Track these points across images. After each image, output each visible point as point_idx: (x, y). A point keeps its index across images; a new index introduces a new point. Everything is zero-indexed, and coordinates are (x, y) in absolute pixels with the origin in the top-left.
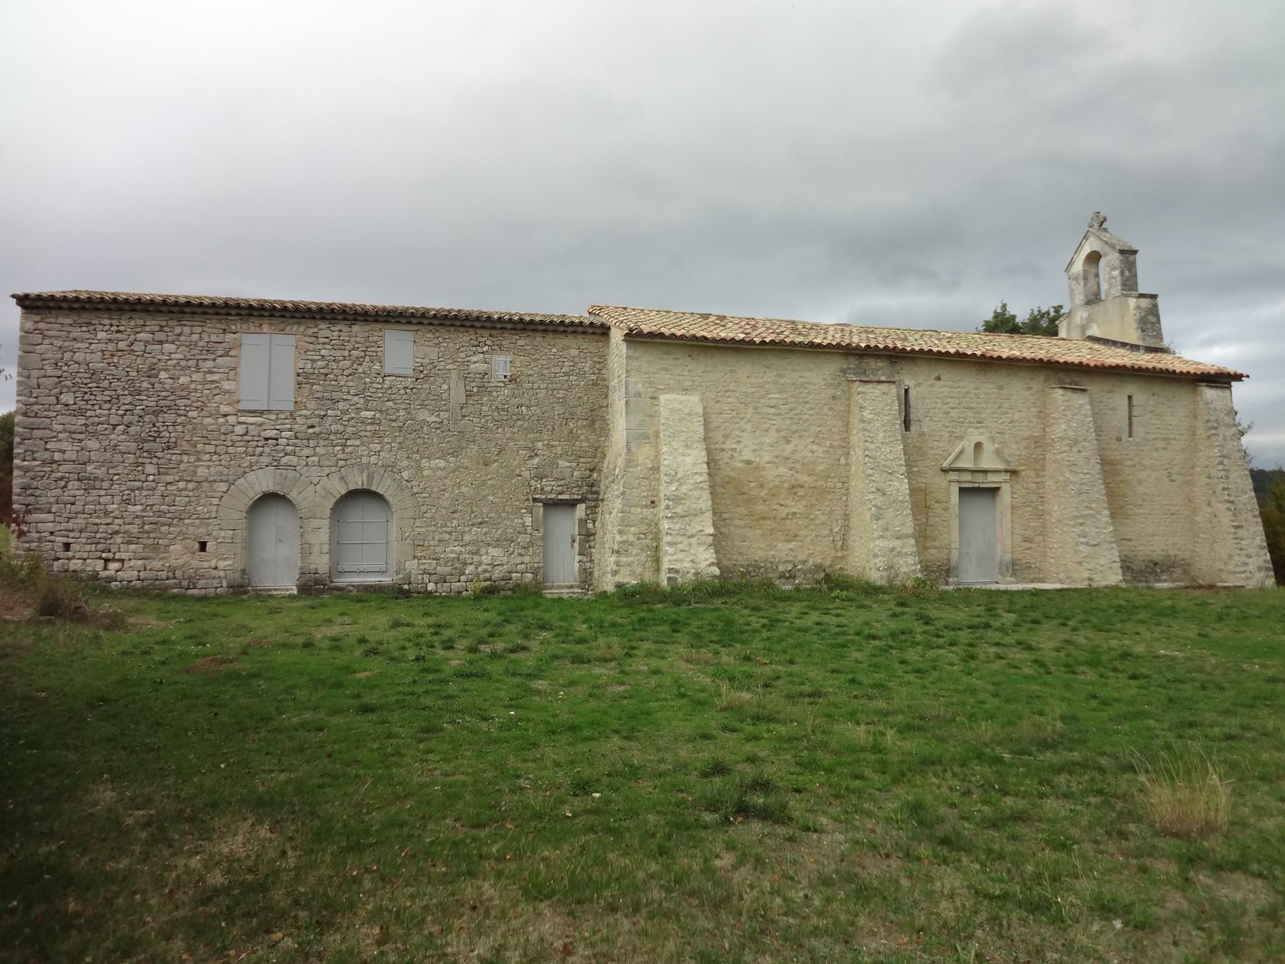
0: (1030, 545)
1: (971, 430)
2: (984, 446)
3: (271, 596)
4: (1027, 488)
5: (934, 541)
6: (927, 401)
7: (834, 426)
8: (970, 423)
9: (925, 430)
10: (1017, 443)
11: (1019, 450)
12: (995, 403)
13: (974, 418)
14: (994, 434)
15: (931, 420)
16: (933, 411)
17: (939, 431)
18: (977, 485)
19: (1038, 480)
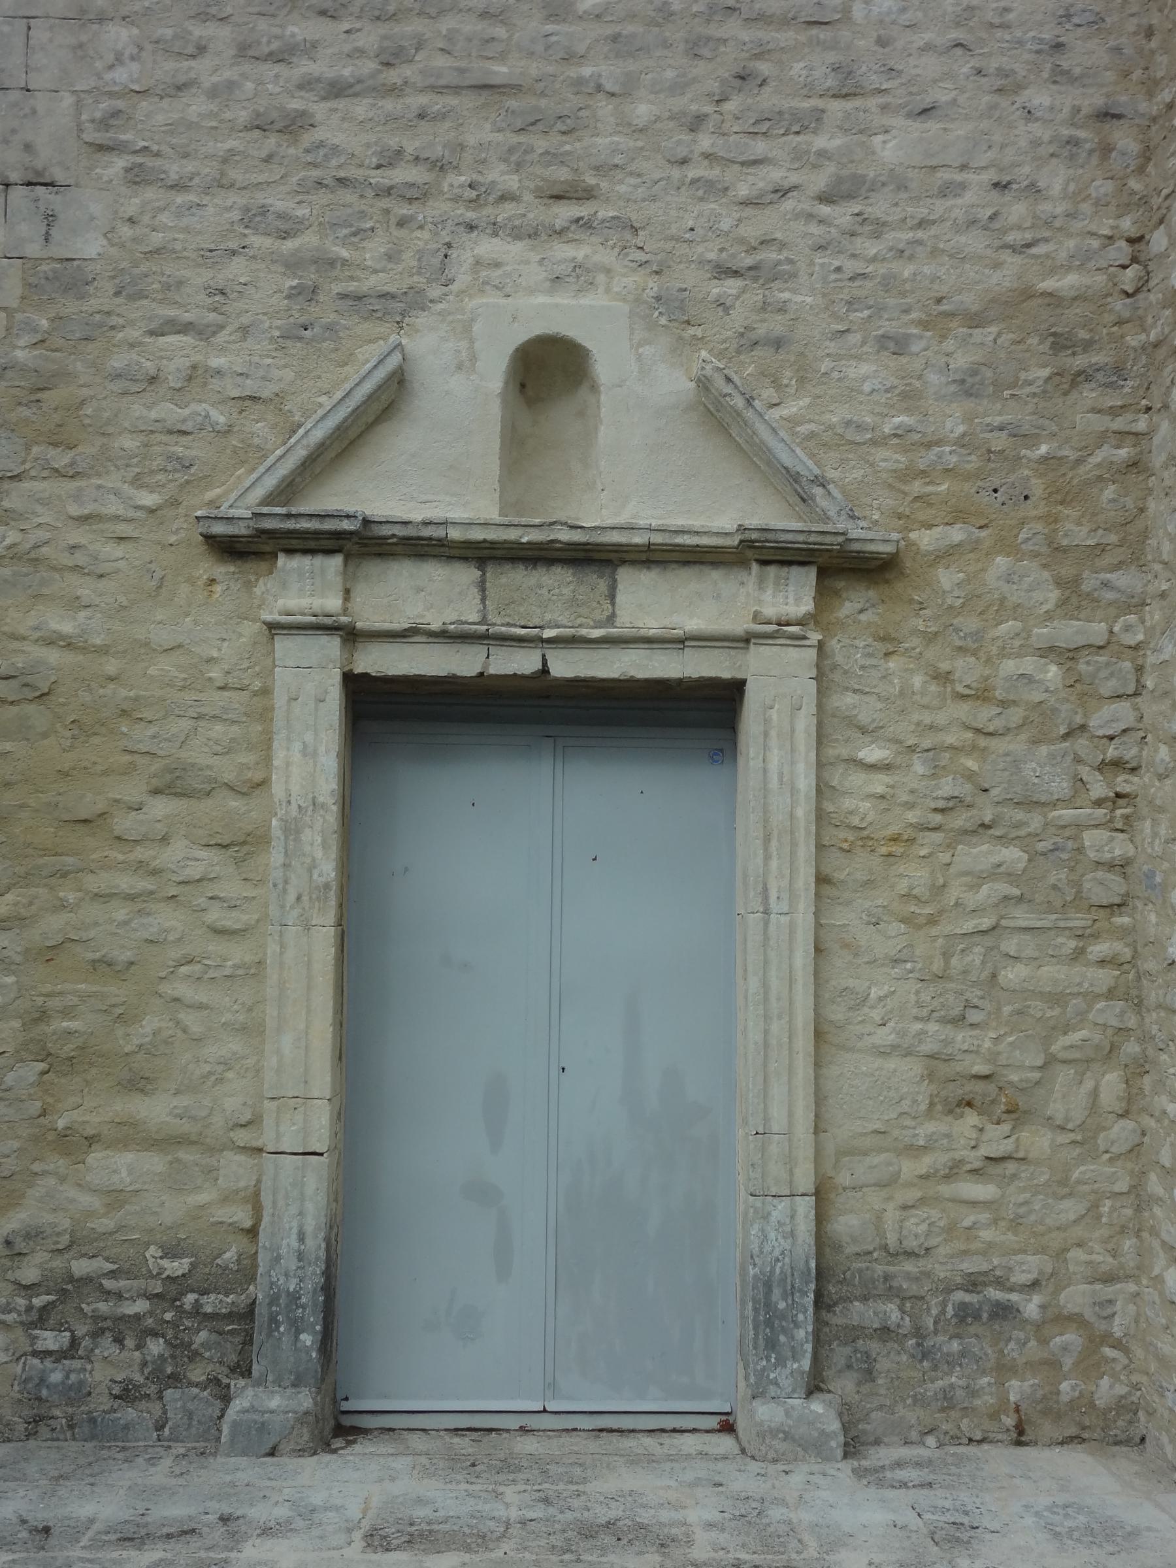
0: (997, 1141)
1: (487, 247)
2: (603, 368)
3: (347, 428)
4: (982, 695)
5: (137, 1084)
6: (119, 35)
7: (918, 1093)
8: (478, 194)
9: (91, 246)
10: (896, 345)
11: (909, 398)
12: (695, 48)
13: (517, 160)
14: (690, 277)
15: (137, 177)
16: (161, 114)
17: (210, 256)
18: (524, 663)
19: (1069, 631)
